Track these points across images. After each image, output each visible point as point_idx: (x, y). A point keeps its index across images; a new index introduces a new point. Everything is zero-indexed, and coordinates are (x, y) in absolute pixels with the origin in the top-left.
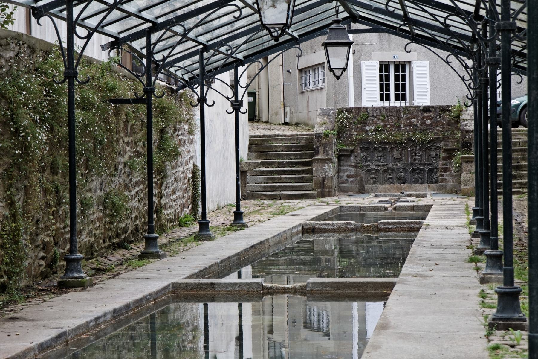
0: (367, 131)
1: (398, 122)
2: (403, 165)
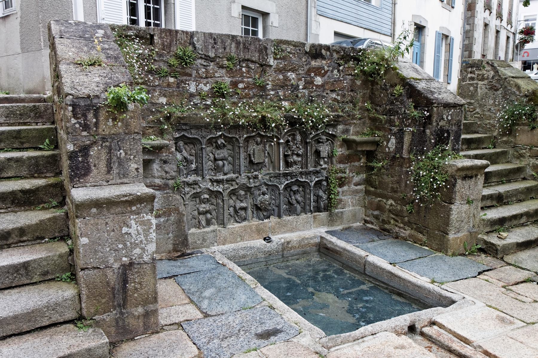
0: (192, 95)
2: (267, 177)
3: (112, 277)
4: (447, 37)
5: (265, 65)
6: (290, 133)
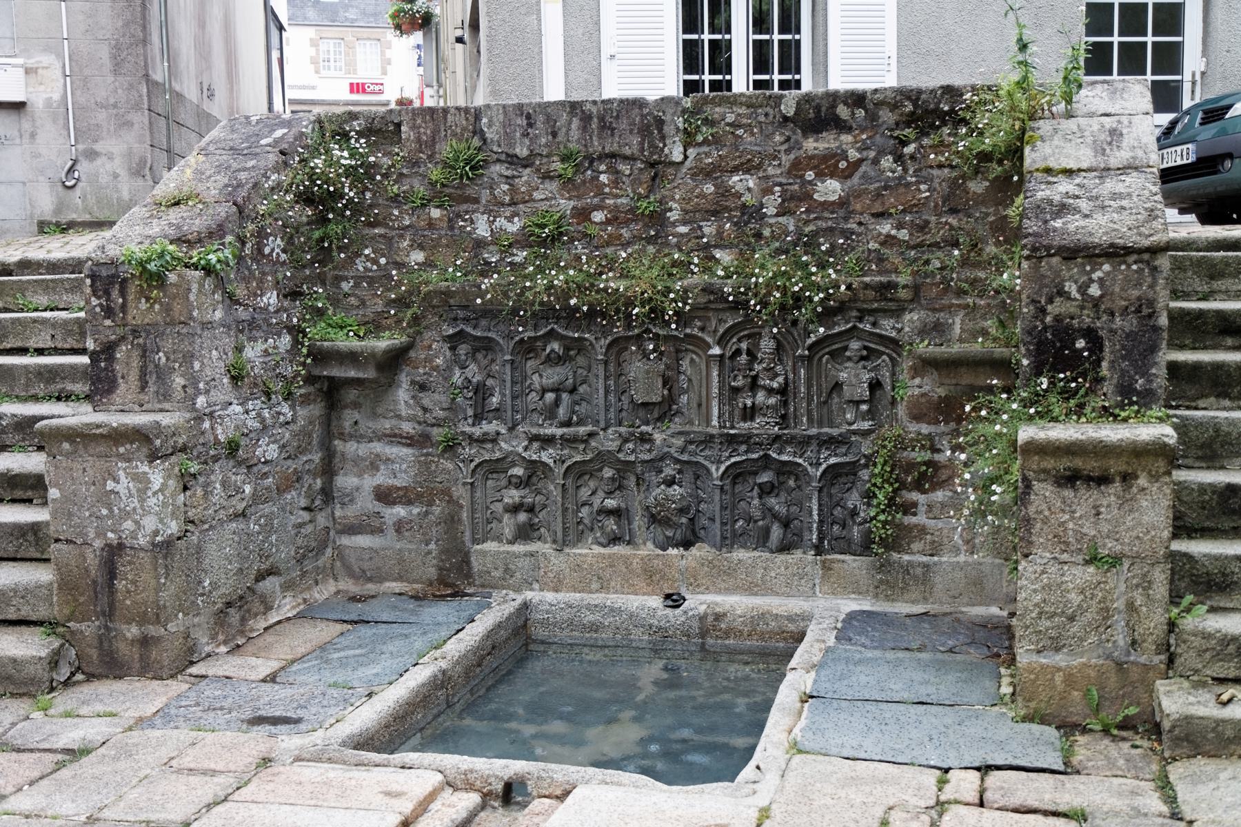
0: (480, 244)
1: (651, 190)
3: (92, 560)
5: (660, 163)
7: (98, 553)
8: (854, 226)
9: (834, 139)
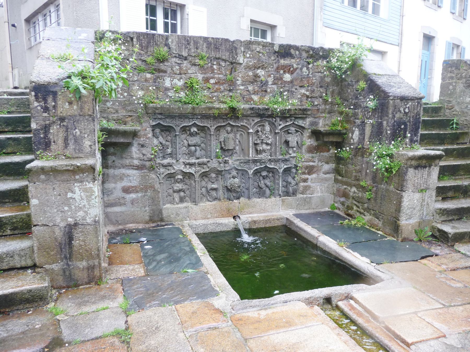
0: (167, 89)
3: (58, 233)
4: (458, 46)
5: (235, 63)
6: (259, 124)
7: (62, 229)
8: (294, 90)
9: (290, 60)
